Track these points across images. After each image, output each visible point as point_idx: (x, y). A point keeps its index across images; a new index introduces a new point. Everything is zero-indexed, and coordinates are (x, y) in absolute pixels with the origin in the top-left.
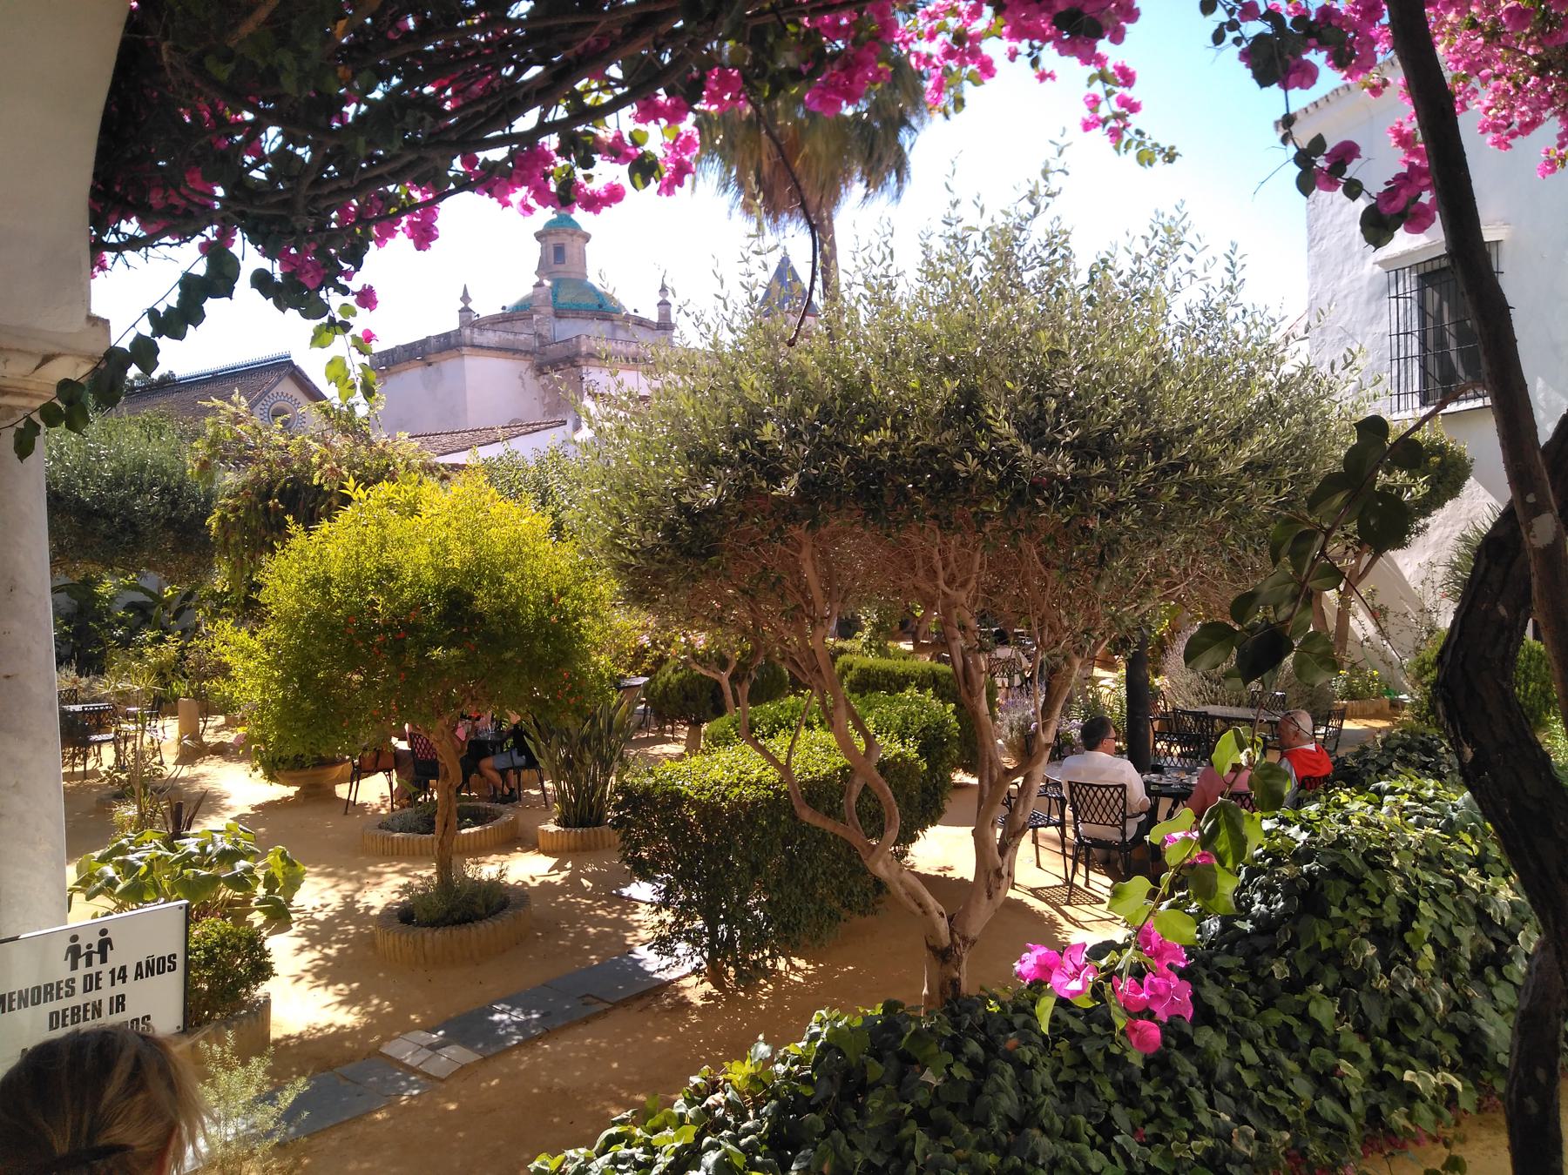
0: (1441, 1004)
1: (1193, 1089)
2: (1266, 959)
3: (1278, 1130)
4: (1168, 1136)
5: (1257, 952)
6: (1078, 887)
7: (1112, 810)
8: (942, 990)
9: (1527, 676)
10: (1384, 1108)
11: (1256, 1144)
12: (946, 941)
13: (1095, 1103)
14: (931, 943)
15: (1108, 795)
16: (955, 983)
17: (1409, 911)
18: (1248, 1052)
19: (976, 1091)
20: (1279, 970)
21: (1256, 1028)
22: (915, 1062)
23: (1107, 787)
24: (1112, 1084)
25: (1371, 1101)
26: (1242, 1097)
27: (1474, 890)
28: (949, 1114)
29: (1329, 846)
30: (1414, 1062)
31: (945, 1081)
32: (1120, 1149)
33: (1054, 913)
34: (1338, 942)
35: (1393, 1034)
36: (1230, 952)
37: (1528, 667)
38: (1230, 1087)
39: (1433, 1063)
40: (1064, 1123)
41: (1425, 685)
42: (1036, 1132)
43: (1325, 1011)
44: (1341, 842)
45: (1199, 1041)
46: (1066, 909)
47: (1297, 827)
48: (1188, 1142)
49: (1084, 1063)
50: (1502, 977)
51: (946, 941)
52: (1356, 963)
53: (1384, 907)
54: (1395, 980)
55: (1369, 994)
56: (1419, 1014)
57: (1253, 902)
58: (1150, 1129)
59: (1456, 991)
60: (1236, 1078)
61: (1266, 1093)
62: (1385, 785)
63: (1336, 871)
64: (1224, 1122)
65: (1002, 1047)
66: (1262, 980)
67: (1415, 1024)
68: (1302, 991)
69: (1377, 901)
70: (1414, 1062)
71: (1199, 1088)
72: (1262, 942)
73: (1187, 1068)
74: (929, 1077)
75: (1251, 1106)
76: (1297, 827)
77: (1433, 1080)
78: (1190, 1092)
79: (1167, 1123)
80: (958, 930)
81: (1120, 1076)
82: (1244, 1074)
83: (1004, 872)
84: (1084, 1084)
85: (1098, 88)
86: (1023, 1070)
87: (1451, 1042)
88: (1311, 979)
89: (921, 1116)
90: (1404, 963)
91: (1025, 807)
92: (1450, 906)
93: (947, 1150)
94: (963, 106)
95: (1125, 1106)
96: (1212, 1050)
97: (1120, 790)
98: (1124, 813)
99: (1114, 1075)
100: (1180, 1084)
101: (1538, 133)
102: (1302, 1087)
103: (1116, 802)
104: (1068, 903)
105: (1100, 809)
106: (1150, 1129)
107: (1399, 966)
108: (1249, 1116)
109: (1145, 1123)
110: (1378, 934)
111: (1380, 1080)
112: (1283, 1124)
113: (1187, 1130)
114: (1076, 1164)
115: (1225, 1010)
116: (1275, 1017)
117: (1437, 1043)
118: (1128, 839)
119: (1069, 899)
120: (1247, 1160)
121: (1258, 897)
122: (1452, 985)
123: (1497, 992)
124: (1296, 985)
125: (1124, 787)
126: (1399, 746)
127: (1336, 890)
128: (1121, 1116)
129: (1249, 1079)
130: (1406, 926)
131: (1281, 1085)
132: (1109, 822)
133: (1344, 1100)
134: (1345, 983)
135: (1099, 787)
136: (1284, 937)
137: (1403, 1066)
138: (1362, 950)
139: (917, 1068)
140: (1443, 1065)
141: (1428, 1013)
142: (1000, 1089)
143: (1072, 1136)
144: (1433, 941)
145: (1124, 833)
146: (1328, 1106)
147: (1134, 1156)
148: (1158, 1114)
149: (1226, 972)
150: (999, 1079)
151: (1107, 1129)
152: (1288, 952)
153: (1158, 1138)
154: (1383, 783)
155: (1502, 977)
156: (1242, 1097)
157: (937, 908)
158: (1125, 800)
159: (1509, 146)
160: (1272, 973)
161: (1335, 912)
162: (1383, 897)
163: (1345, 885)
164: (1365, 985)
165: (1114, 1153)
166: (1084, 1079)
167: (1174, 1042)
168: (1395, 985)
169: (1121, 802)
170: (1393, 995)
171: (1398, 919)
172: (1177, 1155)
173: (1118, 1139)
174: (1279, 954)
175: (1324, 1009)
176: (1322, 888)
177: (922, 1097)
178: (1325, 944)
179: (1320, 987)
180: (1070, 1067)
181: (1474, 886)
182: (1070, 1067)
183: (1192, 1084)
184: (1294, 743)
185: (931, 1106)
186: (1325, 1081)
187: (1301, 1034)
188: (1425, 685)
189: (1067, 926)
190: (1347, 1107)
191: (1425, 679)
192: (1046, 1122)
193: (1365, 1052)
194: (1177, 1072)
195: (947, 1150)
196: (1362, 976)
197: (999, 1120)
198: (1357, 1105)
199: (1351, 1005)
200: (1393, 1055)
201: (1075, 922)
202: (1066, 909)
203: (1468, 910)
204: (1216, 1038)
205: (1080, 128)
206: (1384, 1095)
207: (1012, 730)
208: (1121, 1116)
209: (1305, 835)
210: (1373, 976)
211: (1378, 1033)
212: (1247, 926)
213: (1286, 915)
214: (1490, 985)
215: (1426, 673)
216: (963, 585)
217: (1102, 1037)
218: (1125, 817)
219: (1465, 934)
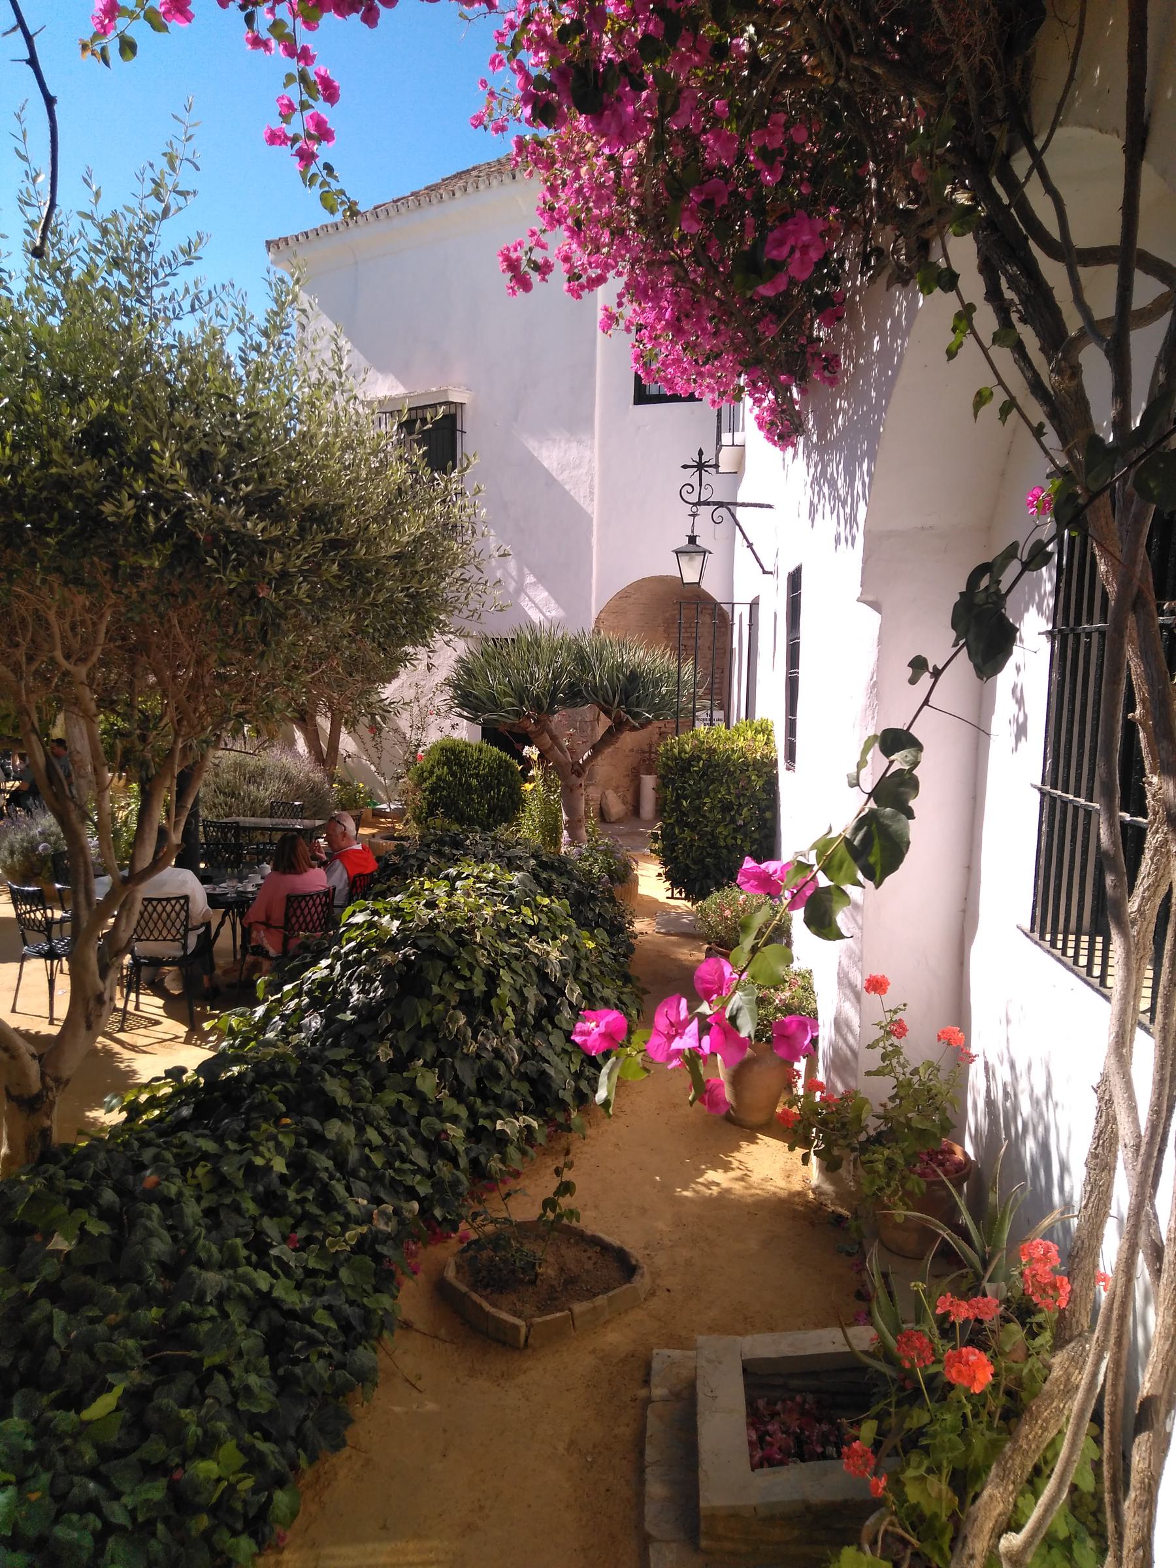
0: (517, 1057)
1: (333, 1182)
2: (374, 1045)
3: (407, 1201)
4: (319, 1234)
5: (362, 1039)
6: (131, 1014)
7: (173, 924)
8: (28, 1144)
9: (499, 781)
10: (482, 1159)
11: (394, 1220)
12: (36, 1086)
13: (242, 1221)
14: (15, 1092)
15: (169, 908)
16: (45, 1133)
17: (492, 979)
18: (372, 1135)
19: (118, 1244)
20: (384, 1053)
21: (378, 1110)
22: (33, 1230)
23: (168, 900)
24: (253, 1199)
25: (473, 1155)
26: (376, 1178)
27: (536, 955)
28: (87, 1279)
29: (422, 931)
30: (500, 1111)
31: (80, 1242)
32: (278, 1259)
33: (108, 1042)
34: (435, 1017)
35: (483, 1093)
36: (336, 1044)
37: (499, 774)
38: (363, 1172)
39: (513, 1109)
40: (221, 1251)
41: (424, 791)
42: (194, 1269)
43: (427, 1082)
44: (432, 926)
45: (330, 1135)
46: (121, 1036)
47: (388, 917)
48: (343, 1234)
49: (222, 1183)
50: (555, 1026)
51: (36, 1086)
52: (450, 1033)
53: (475, 979)
54: (481, 1044)
55: (462, 1059)
56: (502, 1069)
57: (350, 994)
58: (301, 1233)
59: (525, 1043)
60: (366, 1161)
61: (395, 1170)
62: (453, 872)
63: (430, 953)
64: (364, 1206)
65: (138, 1189)
66: (369, 1066)
67: (499, 1078)
68: (406, 1069)
69: (468, 974)
70: (500, 1111)
71: (338, 1180)
72: (364, 1029)
73: (323, 1161)
74: (61, 1243)
75: (384, 1186)
76: (388, 917)
77: (517, 1124)
78: (333, 1186)
79: (314, 1222)
80: (49, 1071)
81: (260, 1188)
82: (373, 1156)
83: (106, 996)
84: (228, 1206)
85: (295, 93)
86: (169, 1205)
87: (525, 1088)
88: (413, 1055)
89: (51, 1291)
90: (486, 1027)
91: (128, 922)
92: (520, 971)
93: (92, 1321)
94: (134, 53)
95: (271, 1217)
96: (345, 1140)
97: (182, 902)
98: (186, 926)
99: (255, 1187)
100: (321, 1180)
101: (600, 290)
102: (419, 1156)
103: (178, 914)
104: (122, 1030)
105: (160, 924)
106: (301, 1233)
107: (485, 1030)
108: (383, 1195)
109: (294, 1228)
110: (468, 1003)
111: (475, 1134)
112: (411, 1194)
113: (339, 1223)
114: (246, 1289)
115: (346, 1101)
116: (390, 1097)
117: (516, 1091)
118: (189, 952)
119: (122, 1026)
120: (388, 1236)
121: (355, 988)
122: (521, 1040)
123: (551, 1038)
124: (400, 1064)
125: (186, 898)
126: (433, 841)
127: (434, 969)
128: (270, 1227)
129: (377, 1160)
130: (490, 993)
131: (404, 1159)
132: (170, 937)
133: (453, 1159)
134: (440, 1054)
135: (159, 900)
136: (384, 1020)
137: (494, 1117)
138: (454, 1020)
139: (38, 1238)
140: (519, 1110)
141: (508, 1067)
142: (151, 1234)
143: (231, 1262)
144: (511, 1003)
145: (185, 947)
146: (443, 1169)
147: (292, 1264)
148: (306, 1216)
149: (338, 1064)
150: (148, 1223)
151: (259, 1246)
152: (390, 1035)
153: (309, 1240)
154: (451, 870)
155: (555, 1026)
156: (376, 1178)
157: (27, 1050)
158: (187, 911)
159: (579, 297)
160: (378, 1058)
161: (436, 989)
162: (471, 968)
163: (441, 965)
164: (458, 1053)
165: (274, 1268)
166: (228, 1201)
167: (305, 1142)
168: (482, 1047)
169: (183, 914)
170: (479, 1056)
171: (484, 988)
172: (333, 1251)
173: (273, 1252)
174: (381, 1039)
175: (428, 1081)
176: (421, 970)
177: (50, 1270)
178: (424, 1021)
179: (421, 1062)
180: (210, 1191)
181: (536, 951)
182: (210, 1191)
183: (331, 1177)
184: (343, 843)
185: (62, 1277)
186: (436, 1146)
187: (409, 1107)
188: (424, 791)
189: (126, 1054)
190: (456, 1165)
191: (424, 786)
192: (203, 1255)
193: (463, 1112)
194: (317, 1169)
195: (92, 1321)
196: (456, 1043)
197: (153, 1267)
198: (463, 1162)
199: (449, 1075)
200: (483, 1110)
201: (134, 1048)
202: (121, 1036)
203: (533, 973)
204: (344, 1128)
205: (262, 137)
206: (482, 1147)
207: (12, 853)
208: (270, 1227)
209: (396, 923)
210: (465, 1043)
211: (470, 1093)
212: (349, 1016)
213: (384, 1001)
214: (549, 1034)
215: (425, 781)
216: (83, 660)
217: (241, 1152)
218: (187, 930)
219: (531, 993)
